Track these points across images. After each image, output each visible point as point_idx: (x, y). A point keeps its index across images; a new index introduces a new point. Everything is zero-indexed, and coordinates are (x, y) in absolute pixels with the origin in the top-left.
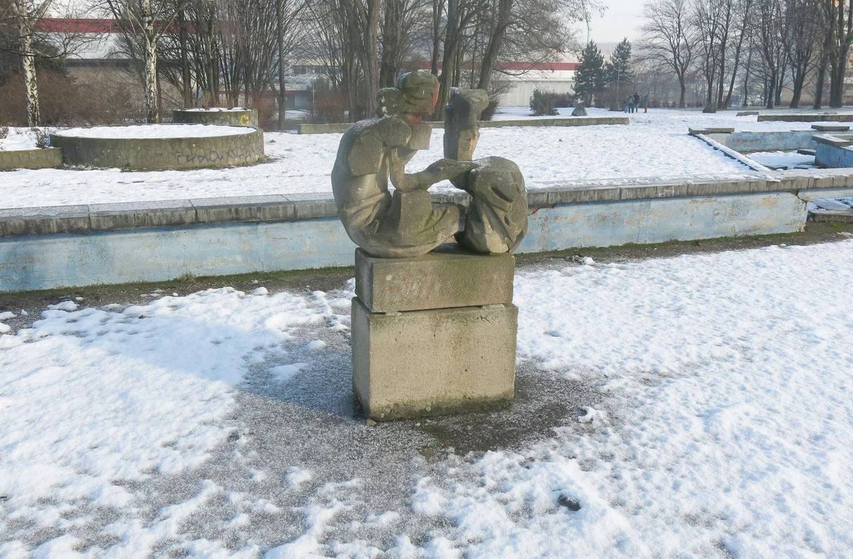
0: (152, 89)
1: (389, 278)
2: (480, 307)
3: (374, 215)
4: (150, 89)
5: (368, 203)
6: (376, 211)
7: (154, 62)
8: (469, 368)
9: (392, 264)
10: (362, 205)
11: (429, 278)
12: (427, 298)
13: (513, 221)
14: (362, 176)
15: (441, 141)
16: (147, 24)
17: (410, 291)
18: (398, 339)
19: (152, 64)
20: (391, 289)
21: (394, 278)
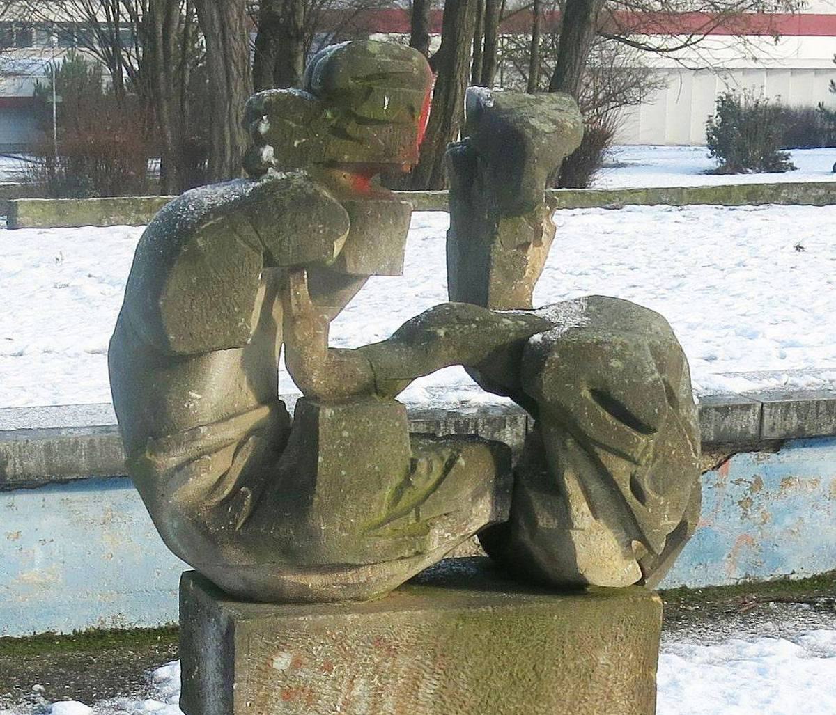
1: (282, 662)
10: (200, 444)
11: (404, 662)
13: (656, 490)
14: (200, 354)
20: (287, 694)
21: (297, 664)
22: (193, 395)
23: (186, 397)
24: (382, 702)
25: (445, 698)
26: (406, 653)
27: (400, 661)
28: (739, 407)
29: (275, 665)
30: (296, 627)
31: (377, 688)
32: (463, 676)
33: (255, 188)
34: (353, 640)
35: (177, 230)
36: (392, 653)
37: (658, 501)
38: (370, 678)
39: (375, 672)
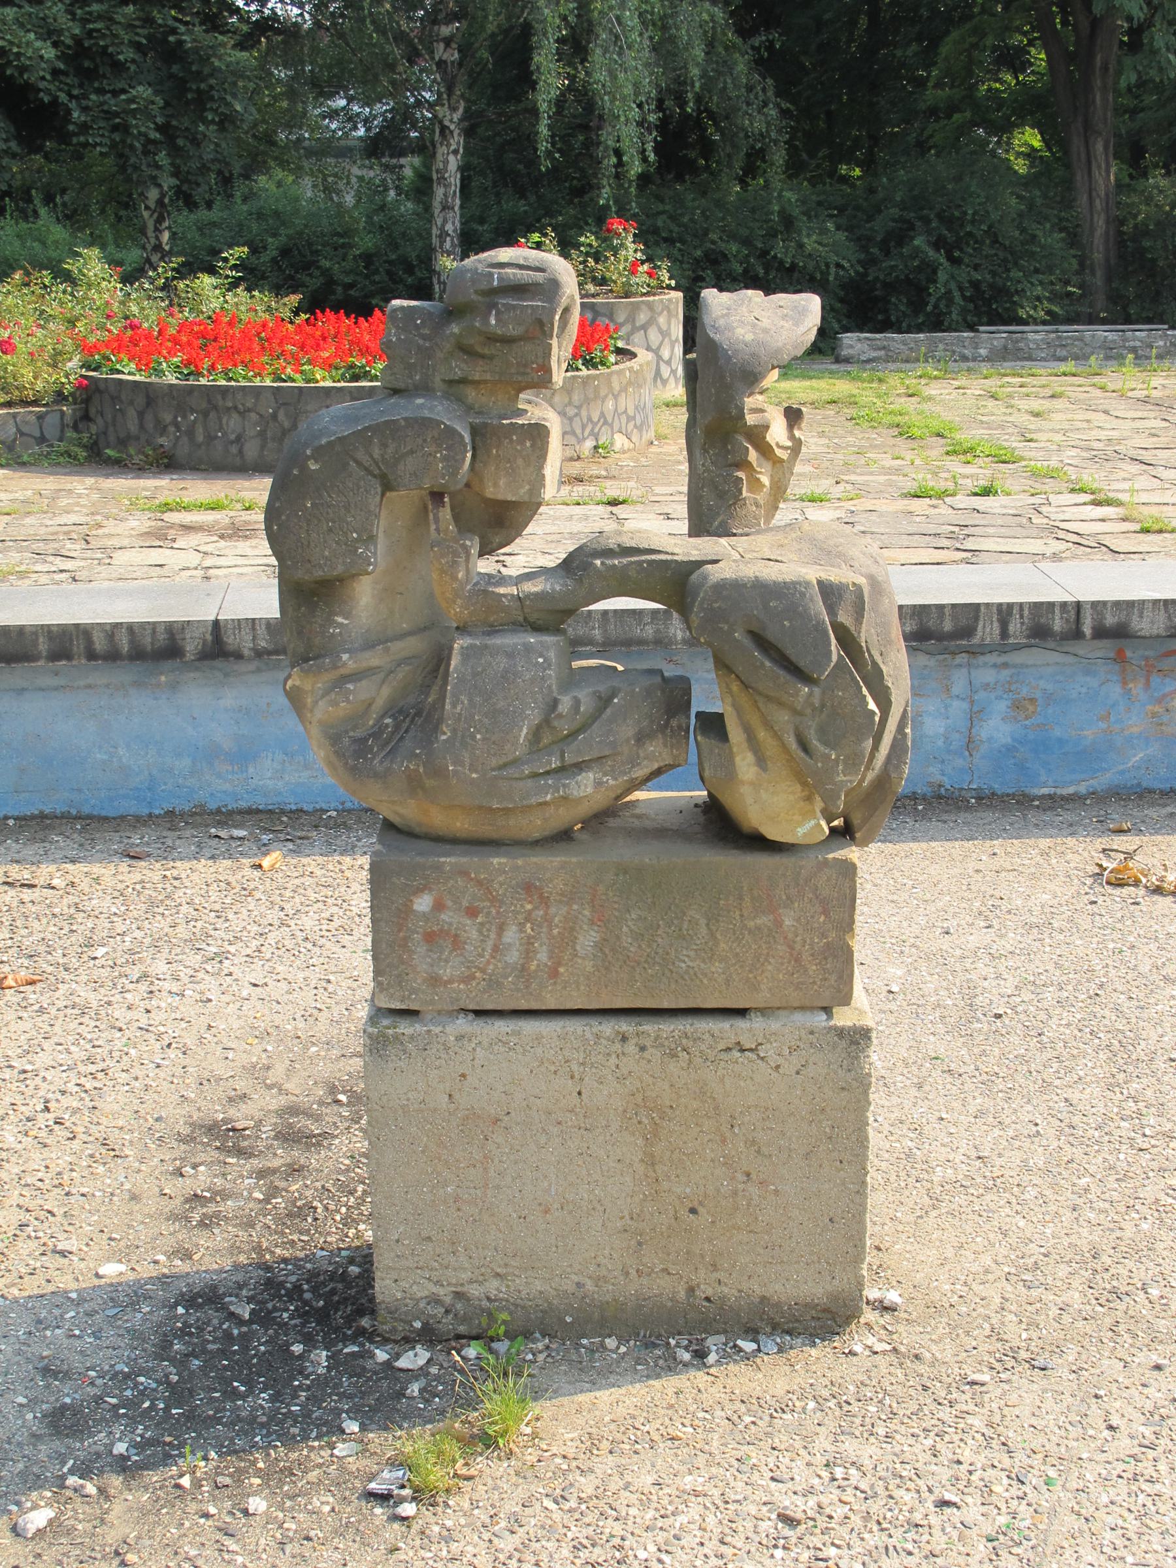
0: (449, 227)
1: (423, 903)
2: (741, 1012)
3: (380, 703)
4: (442, 228)
5: (365, 665)
6: (386, 692)
7: (455, 152)
8: (701, 1203)
9: (432, 860)
10: (343, 671)
11: (558, 913)
12: (554, 974)
13: (826, 744)
14: (353, 576)
15: (959, 396)
16: (442, 45)
17: (496, 949)
18: (457, 1096)
19: (451, 158)
20: (430, 938)
21: (439, 906)
22: (340, 619)
23: (330, 621)
24: (535, 952)
25: (607, 951)
26: (561, 902)
27: (553, 910)
28: (988, 631)
29: (415, 907)
30: (438, 868)
31: (529, 937)
32: (625, 929)
33: (462, 437)
34: (501, 885)
35: (309, 458)
36: (544, 901)
37: (828, 756)
38: (521, 926)
39: (527, 920)
